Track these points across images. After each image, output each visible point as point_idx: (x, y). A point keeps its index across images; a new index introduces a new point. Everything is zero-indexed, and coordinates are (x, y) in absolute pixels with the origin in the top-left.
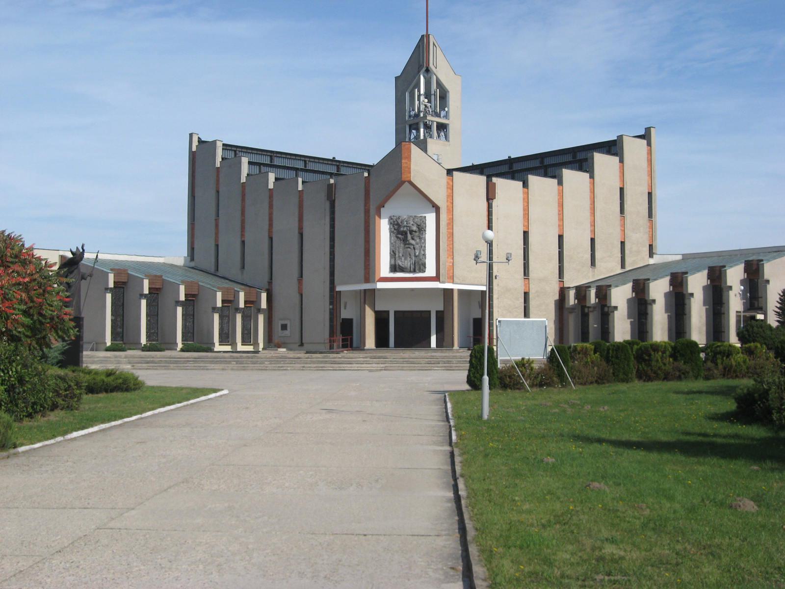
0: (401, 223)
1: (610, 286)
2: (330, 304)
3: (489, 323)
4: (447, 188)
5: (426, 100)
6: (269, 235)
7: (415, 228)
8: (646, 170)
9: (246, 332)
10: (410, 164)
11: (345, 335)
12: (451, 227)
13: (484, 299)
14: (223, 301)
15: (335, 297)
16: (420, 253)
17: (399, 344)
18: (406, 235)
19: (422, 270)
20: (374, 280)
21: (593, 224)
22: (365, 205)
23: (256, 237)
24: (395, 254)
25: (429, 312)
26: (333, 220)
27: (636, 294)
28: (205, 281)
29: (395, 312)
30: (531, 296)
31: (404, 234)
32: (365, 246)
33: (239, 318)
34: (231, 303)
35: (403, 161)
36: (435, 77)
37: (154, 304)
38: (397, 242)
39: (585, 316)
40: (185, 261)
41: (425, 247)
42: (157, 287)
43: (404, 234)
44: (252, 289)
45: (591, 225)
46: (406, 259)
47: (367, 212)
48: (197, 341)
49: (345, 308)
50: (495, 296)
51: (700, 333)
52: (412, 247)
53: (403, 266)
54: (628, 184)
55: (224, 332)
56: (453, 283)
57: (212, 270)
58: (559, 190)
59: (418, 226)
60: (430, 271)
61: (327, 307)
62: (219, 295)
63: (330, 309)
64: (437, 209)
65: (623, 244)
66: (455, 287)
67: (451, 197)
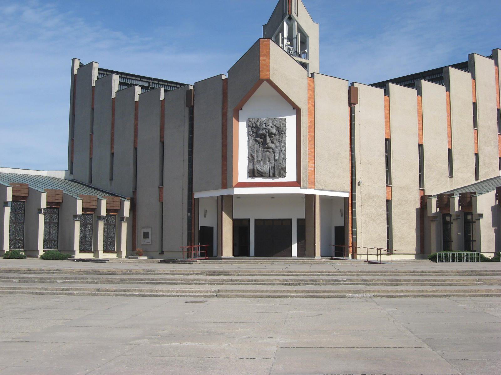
0: (260, 125)
1: (475, 193)
2: (188, 212)
3: (352, 231)
4: (308, 89)
5: (289, 43)
6: (134, 146)
7: (274, 131)
8: (495, 87)
9: (110, 240)
10: (269, 62)
11: (204, 244)
12: (312, 130)
13: (346, 207)
14: (84, 209)
15: (193, 205)
16: (279, 157)
17: (259, 253)
18: (265, 138)
19: (282, 175)
20: (232, 186)
21: (450, 136)
22: (223, 109)
23: (124, 148)
24: (254, 158)
25: (290, 220)
26: (191, 126)
27: (499, 202)
28: (73, 190)
29: (256, 220)
30: (393, 204)
31: (263, 137)
32: (223, 150)
33: (101, 225)
34: (117, 213)
35: (261, 58)
36: (296, 24)
37: (19, 212)
38: (256, 145)
39: (446, 226)
40: (66, 174)
41: (285, 150)
42: (23, 195)
43: (263, 137)
44: (116, 197)
45: (448, 137)
46: (264, 163)
47: (225, 115)
48: (59, 248)
49: (205, 216)
50: (358, 204)
52: (271, 151)
53: (262, 171)
54: (479, 99)
55: (87, 240)
56: (315, 188)
57: (87, 182)
58: (418, 100)
59: (278, 128)
60: (291, 175)
61: (185, 214)
62: (80, 203)
63: (188, 217)
64: (297, 111)
65: (477, 155)
67: (312, 99)
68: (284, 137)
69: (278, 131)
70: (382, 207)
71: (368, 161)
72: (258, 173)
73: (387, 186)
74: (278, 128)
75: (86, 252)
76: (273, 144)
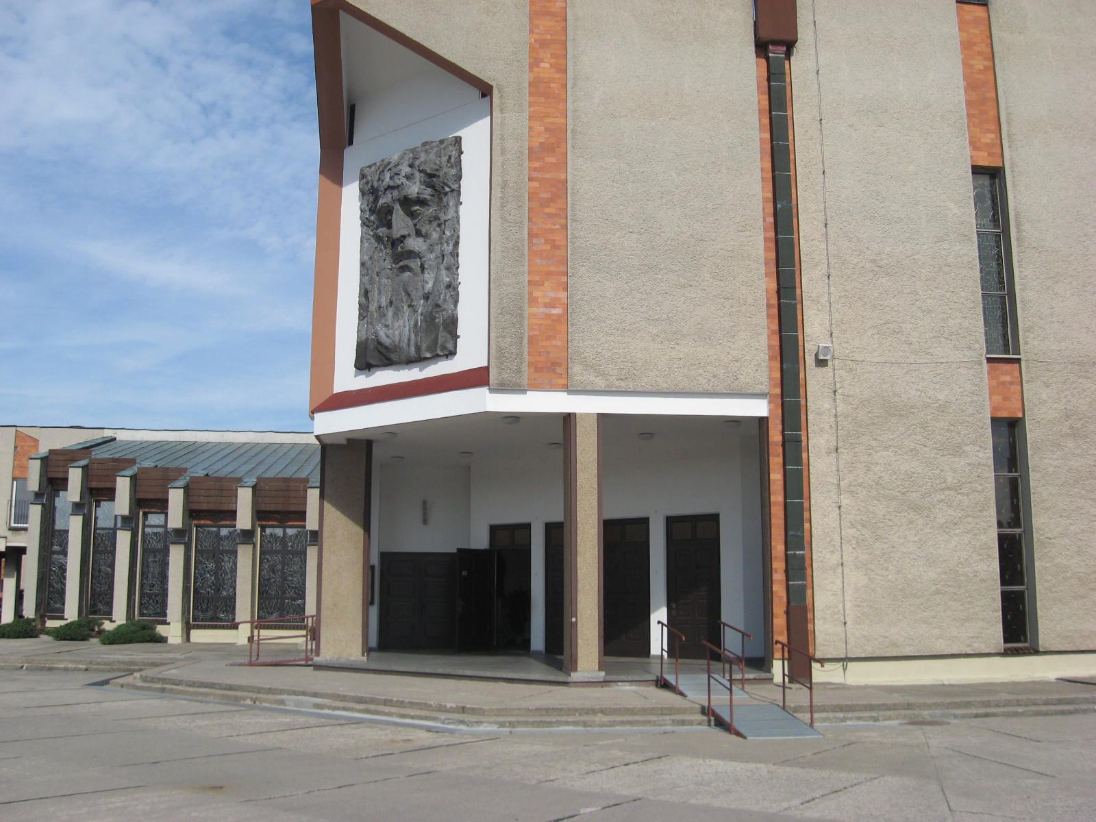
19: (444, 348)
25: (644, 522)
29: (671, 521)
30: (1033, 435)
41: (455, 255)
46: (396, 315)
51: (910, 651)
59: (431, 179)
66: (586, 406)
68: (451, 203)
69: (433, 187)
70: (967, 448)
71: (874, 261)
72: (379, 351)
73: (989, 360)
74: (431, 176)
75: (215, 627)
76: (421, 240)
